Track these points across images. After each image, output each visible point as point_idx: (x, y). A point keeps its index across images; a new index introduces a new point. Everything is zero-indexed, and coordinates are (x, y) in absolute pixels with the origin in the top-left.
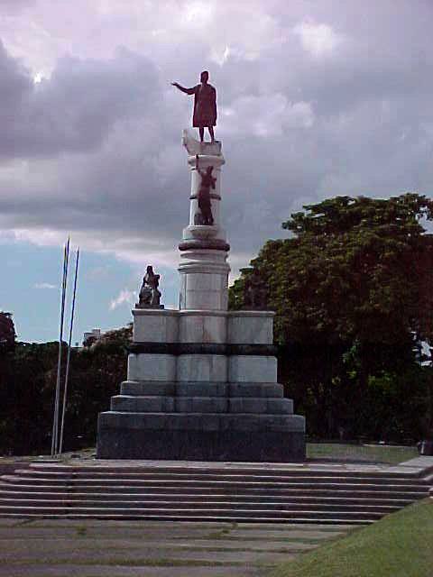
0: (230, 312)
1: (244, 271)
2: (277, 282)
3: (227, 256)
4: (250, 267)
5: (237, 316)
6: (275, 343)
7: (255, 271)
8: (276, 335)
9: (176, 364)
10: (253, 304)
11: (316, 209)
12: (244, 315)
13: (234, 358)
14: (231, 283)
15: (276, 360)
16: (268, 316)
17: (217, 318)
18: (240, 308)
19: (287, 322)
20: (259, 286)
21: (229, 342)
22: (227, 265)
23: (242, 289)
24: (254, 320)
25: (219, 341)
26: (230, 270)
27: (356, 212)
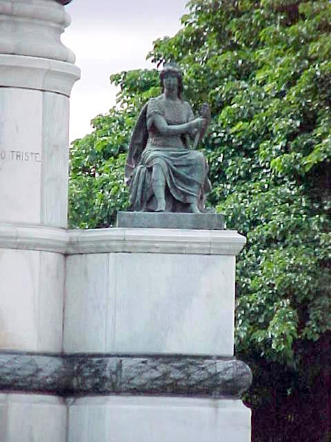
0: (77, 234)
1: (132, 84)
2: (255, 125)
3: (63, 24)
4: (152, 66)
5: (102, 249)
6: (246, 351)
7: (174, 86)
8: (252, 317)
9: (68, 412)
10: (162, 203)
11: (75, 228)
12: (127, 248)
13: (87, 407)
14: (80, 128)
15: (251, 412)
16: (209, 251)
17: (35, 255)
18: (109, 220)
19: (295, 269)
20: (184, 137)
21: (69, 350)
22: (66, 58)
23: (122, 150)
24: (165, 266)
25: (32, 345)
26: (79, 79)
27: (250, 121)
